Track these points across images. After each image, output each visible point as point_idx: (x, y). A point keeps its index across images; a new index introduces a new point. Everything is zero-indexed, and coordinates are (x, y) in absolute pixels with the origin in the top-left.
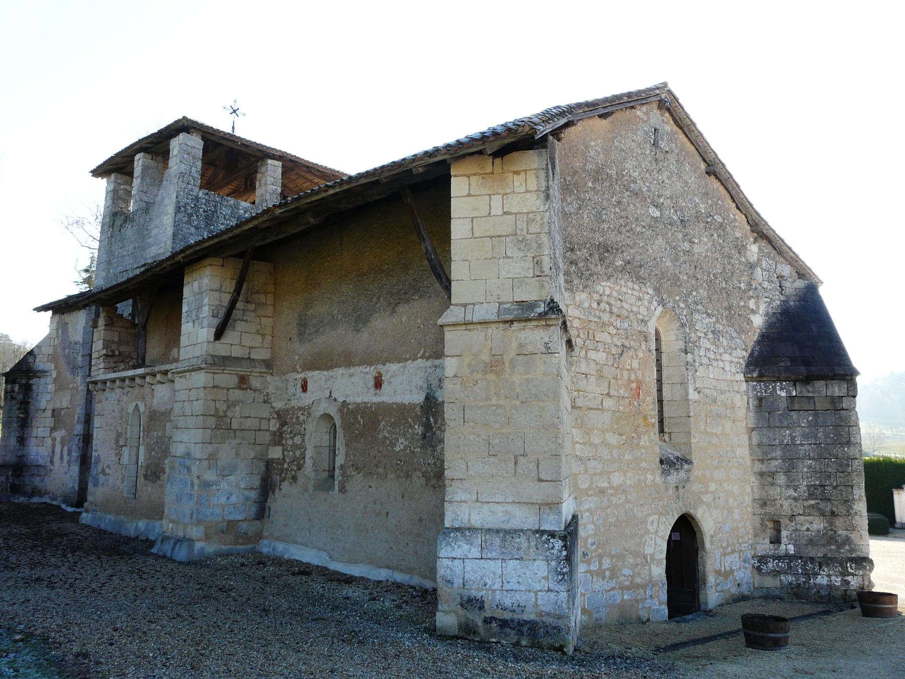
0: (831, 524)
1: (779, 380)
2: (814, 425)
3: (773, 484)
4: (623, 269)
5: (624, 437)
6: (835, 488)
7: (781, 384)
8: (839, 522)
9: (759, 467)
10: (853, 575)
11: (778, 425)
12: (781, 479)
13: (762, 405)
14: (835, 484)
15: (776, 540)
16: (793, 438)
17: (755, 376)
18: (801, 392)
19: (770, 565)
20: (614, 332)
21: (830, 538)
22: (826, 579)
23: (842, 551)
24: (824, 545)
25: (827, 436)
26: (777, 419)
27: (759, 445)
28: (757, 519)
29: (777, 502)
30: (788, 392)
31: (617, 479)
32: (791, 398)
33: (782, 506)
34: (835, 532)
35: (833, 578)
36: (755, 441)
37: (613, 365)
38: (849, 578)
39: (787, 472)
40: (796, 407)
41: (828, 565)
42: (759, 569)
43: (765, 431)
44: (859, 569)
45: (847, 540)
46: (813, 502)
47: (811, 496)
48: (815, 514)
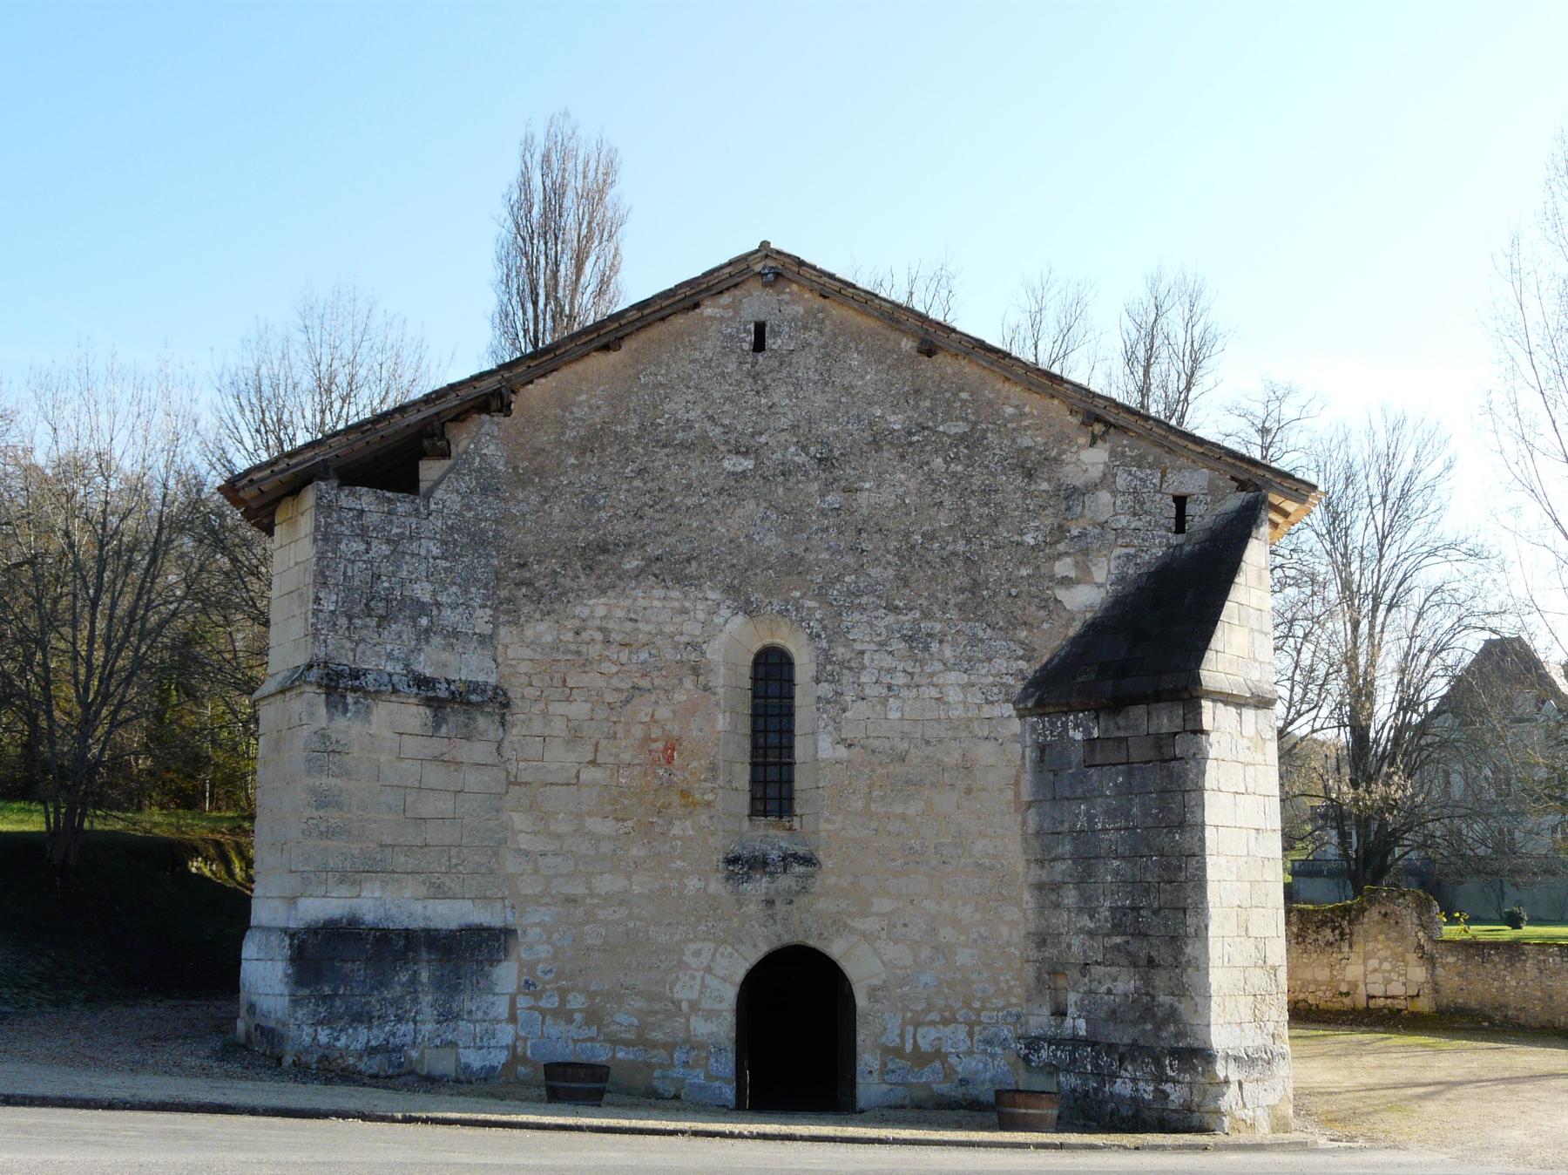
0: (1147, 981)
1: (1075, 711)
2: (1125, 792)
3: (1057, 906)
4: (639, 574)
5: (629, 823)
6: (1156, 912)
7: (1076, 717)
8: (1160, 979)
9: (1036, 874)
10: (1175, 1081)
11: (1067, 794)
12: (1071, 897)
13: (1046, 757)
14: (1156, 905)
15: (1060, 1013)
16: (1091, 818)
17: (1030, 705)
18: (1107, 730)
19: (1044, 1053)
20: (614, 669)
21: (1145, 1009)
22: (1130, 1085)
23: (1164, 1034)
24: (1134, 1023)
25: (1146, 814)
26: (1066, 781)
27: (1037, 834)
28: (1030, 971)
29: (1062, 939)
30: (1087, 731)
31: (606, 883)
32: (1090, 742)
33: (1069, 946)
34: (1153, 998)
35: (1141, 1085)
36: (1032, 826)
37: (607, 719)
38: (1168, 1087)
39: (1080, 883)
40: (1098, 759)
41: (1134, 1060)
42: (1026, 1060)
43: (1048, 805)
44: (1185, 1071)
45: (1173, 1015)
46: (1118, 940)
47: (1117, 928)
48: (1122, 961)
